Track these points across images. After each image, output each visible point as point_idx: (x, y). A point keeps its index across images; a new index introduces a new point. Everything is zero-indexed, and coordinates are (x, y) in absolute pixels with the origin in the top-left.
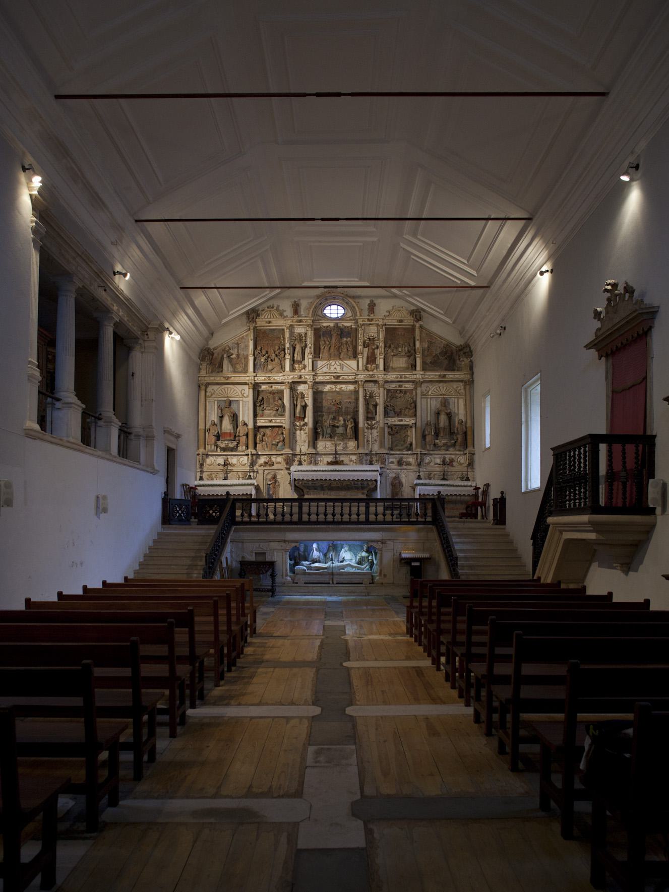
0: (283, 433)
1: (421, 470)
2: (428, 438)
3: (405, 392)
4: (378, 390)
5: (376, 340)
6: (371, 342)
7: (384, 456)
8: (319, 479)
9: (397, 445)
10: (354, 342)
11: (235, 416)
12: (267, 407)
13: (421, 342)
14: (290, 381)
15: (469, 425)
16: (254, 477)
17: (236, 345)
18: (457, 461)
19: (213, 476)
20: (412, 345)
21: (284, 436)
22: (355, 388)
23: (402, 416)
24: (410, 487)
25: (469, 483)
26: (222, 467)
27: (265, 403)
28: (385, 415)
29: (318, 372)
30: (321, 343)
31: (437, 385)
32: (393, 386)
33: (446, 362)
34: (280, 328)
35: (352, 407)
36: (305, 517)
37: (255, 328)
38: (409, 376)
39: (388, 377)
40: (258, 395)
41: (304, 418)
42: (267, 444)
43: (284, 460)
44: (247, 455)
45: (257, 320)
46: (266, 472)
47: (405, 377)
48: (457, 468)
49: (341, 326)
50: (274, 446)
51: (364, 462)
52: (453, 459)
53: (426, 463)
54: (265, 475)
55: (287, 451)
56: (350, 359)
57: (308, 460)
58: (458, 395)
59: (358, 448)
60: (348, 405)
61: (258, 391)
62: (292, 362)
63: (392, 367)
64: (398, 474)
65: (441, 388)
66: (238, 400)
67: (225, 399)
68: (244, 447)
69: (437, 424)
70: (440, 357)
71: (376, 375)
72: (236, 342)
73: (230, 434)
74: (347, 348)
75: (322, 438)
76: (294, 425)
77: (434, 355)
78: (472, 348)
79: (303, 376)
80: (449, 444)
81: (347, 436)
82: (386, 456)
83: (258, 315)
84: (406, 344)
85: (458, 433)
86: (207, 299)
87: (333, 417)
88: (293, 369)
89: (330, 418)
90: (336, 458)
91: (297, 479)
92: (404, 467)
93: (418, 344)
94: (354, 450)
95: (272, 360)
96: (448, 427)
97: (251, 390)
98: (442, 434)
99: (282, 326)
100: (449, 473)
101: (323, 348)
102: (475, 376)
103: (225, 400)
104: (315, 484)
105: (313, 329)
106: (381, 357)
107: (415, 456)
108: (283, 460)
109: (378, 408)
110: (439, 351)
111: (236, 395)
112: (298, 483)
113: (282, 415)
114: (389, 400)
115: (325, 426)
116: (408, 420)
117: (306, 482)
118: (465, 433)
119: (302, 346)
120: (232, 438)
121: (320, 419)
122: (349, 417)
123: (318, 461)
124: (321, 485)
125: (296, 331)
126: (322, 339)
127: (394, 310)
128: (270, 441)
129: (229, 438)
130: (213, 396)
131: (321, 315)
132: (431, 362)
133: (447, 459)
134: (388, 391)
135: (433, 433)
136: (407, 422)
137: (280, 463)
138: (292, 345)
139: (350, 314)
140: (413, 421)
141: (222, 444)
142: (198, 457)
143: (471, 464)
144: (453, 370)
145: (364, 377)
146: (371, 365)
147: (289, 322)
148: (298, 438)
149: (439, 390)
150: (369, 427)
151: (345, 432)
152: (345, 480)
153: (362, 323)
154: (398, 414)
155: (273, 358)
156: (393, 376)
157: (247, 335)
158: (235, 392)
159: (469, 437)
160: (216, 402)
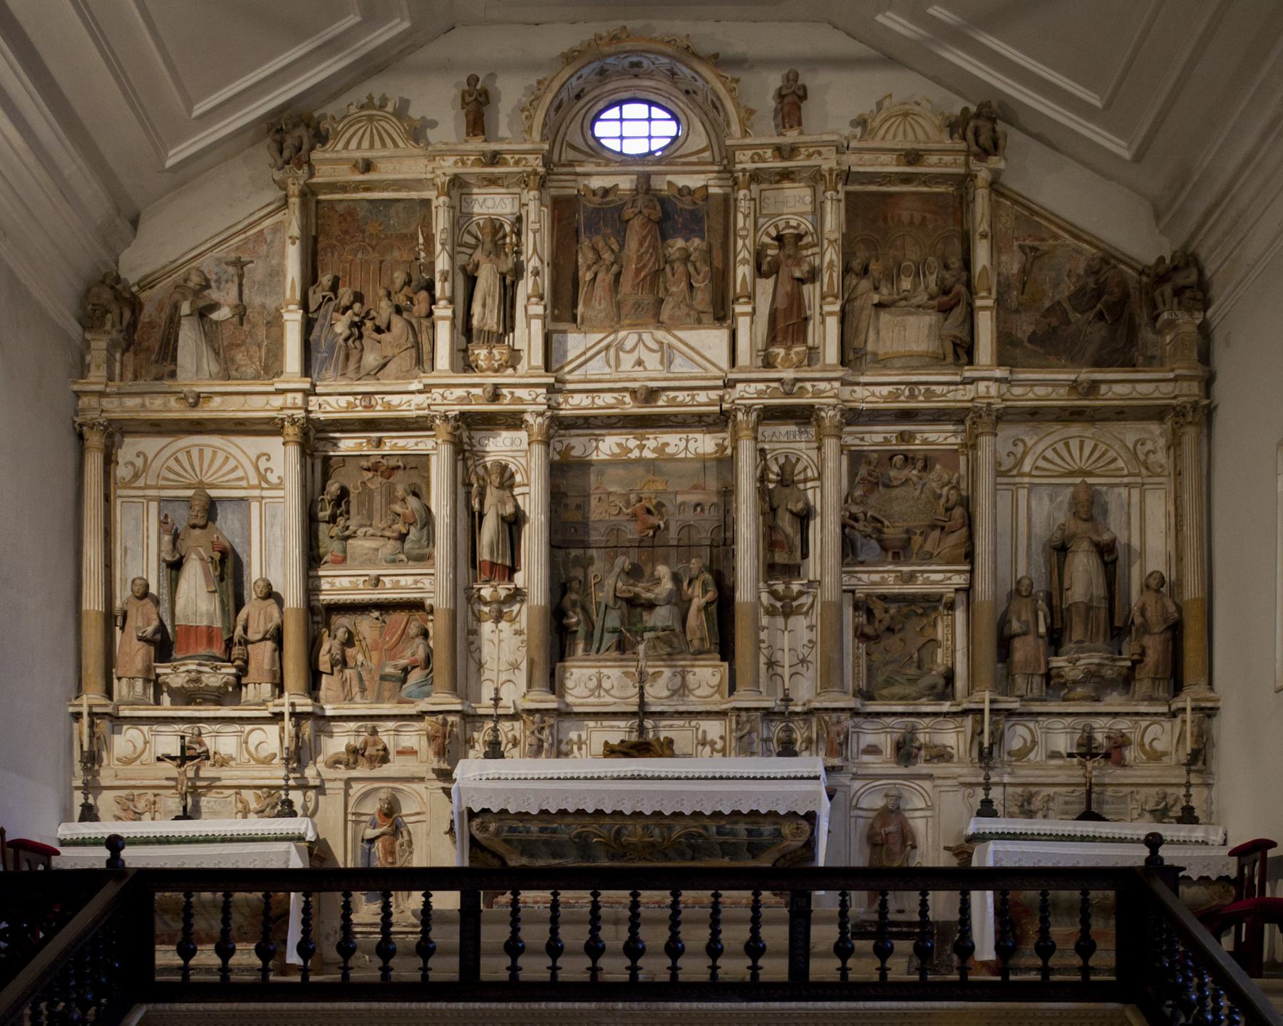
0: (425, 634)
1: (993, 780)
2: (1022, 650)
3: (926, 460)
4: (814, 454)
5: (807, 247)
6: (790, 250)
7: (839, 722)
8: (571, 810)
9: (889, 682)
10: (717, 254)
11: (230, 563)
12: (362, 526)
13: (995, 250)
14: (455, 410)
15: (1192, 590)
16: (305, 808)
17: (231, 270)
18: (1142, 745)
19: (141, 805)
20: (955, 262)
21: (431, 643)
22: (721, 447)
23: (914, 559)
24: (946, 848)
25: (1198, 833)
26: (170, 768)
27: (353, 510)
28: (844, 555)
29: (568, 377)
30: (580, 261)
31: (1059, 432)
32: (876, 437)
33: (1098, 332)
34: (414, 195)
35: (709, 526)
36: (494, 968)
37: (308, 193)
38: (945, 388)
39: (860, 392)
40: (326, 477)
41: (513, 570)
42: (361, 679)
43: (431, 738)
44: (277, 717)
45: (316, 155)
46: (357, 789)
47: (929, 395)
48: (1138, 771)
49: (665, 187)
50: (387, 685)
51: (758, 746)
52: (1123, 735)
53: (1009, 753)
54: (351, 802)
55: (442, 700)
56: (699, 323)
57: (528, 740)
58: (1144, 471)
59: (732, 689)
60: (689, 516)
61: (327, 459)
62: (463, 340)
63: (875, 354)
64: (899, 797)
65: (1074, 444)
66: (241, 499)
67: (190, 493)
68: (267, 688)
69: (1055, 593)
70: (1075, 316)
71: (808, 385)
72: (233, 256)
73: (210, 632)
74: (689, 276)
75: (587, 650)
76: (469, 599)
77: (1047, 304)
78: (1208, 274)
79: (505, 391)
80: (1108, 673)
81: (688, 643)
82: (850, 723)
83: (321, 138)
84: (931, 259)
85: (1145, 629)
86: (117, 78)
87: (627, 566)
88: (464, 362)
89: (617, 570)
90: (642, 730)
91: (476, 810)
92: (921, 767)
93: (982, 255)
94: (717, 697)
95: (378, 330)
96: (1104, 605)
97: (293, 451)
98: (1077, 632)
99: (418, 184)
100: (1110, 791)
101: (589, 276)
102: (1219, 388)
103: (187, 500)
104: (554, 831)
105: (548, 201)
106: (827, 308)
107: (969, 722)
108: (424, 740)
109: (814, 526)
110: (1067, 288)
111: (232, 476)
112: (483, 828)
113: (424, 558)
114: (858, 493)
115: (598, 604)
116: (939, 577)
117: (515, 824)
118: (1175, 630)
119: (504, 269)
120: (218, 651)
121: (578, 572)
122: (695, 564)
123: (570, 742)
124: (579, 835)
125: (476, 209)
126: (585, 242)
127: (883, 115)
128: (372, 665)
129: (203, 651)
130: (141, 482)
131: (586, 149)
132: (1034, 333)
133: (1100, 737)
134: (856, 458)
135: (1042, 629)
136: (934, 583)
137: (412, 752)
138: (463, 269)
139: (699, 140)
140: (960, 580)
141: (176, 676)
142: (76, 725)
143: (1199, 758)
144: (1130, 364)
145: (760, 394)
146: (789, 349)
147: (448, 166)
148: (488, 652)
149: (1065, 454)
150: (779, 604)
151: (678, 628)
152: (681, 814)
153: (750, 166)
154: (898, 551)
155: (382, 322)
156: (877, 389)
157: (277, 228)
158: (232, 463)
159: (1192, 645)
160: (154, 506)
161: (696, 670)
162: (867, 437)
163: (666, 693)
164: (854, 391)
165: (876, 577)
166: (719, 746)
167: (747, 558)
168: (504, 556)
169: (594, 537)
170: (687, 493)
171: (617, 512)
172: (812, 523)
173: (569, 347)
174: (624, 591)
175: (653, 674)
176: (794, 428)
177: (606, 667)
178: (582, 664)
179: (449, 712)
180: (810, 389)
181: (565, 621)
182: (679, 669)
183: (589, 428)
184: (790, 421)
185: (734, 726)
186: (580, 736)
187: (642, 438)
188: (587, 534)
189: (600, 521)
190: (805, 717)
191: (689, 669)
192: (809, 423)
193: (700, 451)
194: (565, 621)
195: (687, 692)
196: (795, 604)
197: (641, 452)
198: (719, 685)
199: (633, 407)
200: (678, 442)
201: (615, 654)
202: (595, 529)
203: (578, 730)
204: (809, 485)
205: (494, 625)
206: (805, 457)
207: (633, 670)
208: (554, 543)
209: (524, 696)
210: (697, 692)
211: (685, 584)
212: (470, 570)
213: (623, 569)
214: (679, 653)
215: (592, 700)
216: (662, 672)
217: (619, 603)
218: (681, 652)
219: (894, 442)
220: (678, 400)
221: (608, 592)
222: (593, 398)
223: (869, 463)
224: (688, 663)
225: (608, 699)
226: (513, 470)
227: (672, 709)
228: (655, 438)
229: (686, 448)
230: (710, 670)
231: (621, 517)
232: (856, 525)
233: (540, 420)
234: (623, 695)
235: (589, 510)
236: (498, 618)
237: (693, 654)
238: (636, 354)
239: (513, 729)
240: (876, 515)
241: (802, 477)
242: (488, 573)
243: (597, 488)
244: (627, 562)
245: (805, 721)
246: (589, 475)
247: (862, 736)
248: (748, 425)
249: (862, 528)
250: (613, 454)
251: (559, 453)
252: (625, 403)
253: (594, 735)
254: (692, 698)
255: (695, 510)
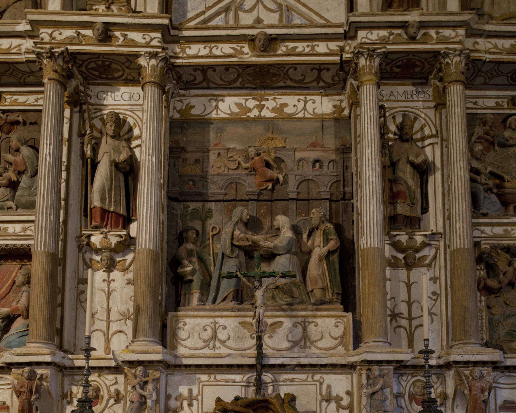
22: (339, 109)
59: (357, 341)
60: (308, 171)
71: (432, 32)
75: (202, 300)
87: (245, 217)
89: (235, 219)
90: (259, 384)
94: (341, 349)
115: (215, 255)
121: (197, 225)
145: (384, 41)
150: (401, 256)
161: (318, 320)
162: (480, 101)
163: (286, 345)
164: (477, 43)
165: (498, 230)
166: (345, 402)
167: (373, 202)
168: (117, 203)
169: (213, 190)
170: (305, 150)
171: (234, 167)
172: (431, 179)
173: (189, 8)
174: (242, 239)
175: (272, 325)
176: (411, 88)
177: (222, 317)
178: (196, 313)
179: (39, 364)
180: (435, 36)
181: (179, 270)
182: (300, 320)
183: (208, 88)
184: (406, 81)
185: (364, 381)
186: (190, 391)
187: (261, 99)
188: (206, 187)
189: (218, 175)
190: (438, 371)
191: (310, 320)
192: (426, 84)
193: (318, 111)
194: (179, 270)
195: (308, 344)
196: (418, 255)
197: (260, 112)
198: (343, 337)
199: (251, 57)
200: (296, 103)
201: (233, 304)
202: (214, 183)
203: (189, 384)
204: (427, 142)
205: (105, 274)
206: (423, 115)
207: (250, 320)
208: (171, 195)
209: (127, 347)
210: (320, 344)
211: (305, 236)
212: (83, 218)
213: (241, 218)
214: (299, 303)
215: (207, 351)
216: (281, 323)
217: (237, 252)
218: (302, 302)
219: (506, 106)
220: (298, 50)
221: (225, 240)
222: (211, 49)
223: (485, 123)
224: (310, 313)
225: (224, 351)
226: (132, 124)
227: (294, 362)
228: (274, 99)
229: (305, 108)
230: (333, 321)
231: (239, 172)
232: (478, 178)
233: (153, 62)
234: (240, 346)
235: (208, 165)
236: (110, 267)
237: (314, 304)
238: (255, 14)
239: (116, 383)
240: (495, 170)
241: (419, 136)
242: (99, 220)
243: (216, 145)
244: (246, 211)
245: (438, 375)
246: (209, 131)
247: (499, 391)
248: (370, 70)
249: (484, 181)
250: (232, 113)
251: (178, 112)
252: (243, 53)
253: (206, 389)
254: (314, 350)
255: (314, 166)
